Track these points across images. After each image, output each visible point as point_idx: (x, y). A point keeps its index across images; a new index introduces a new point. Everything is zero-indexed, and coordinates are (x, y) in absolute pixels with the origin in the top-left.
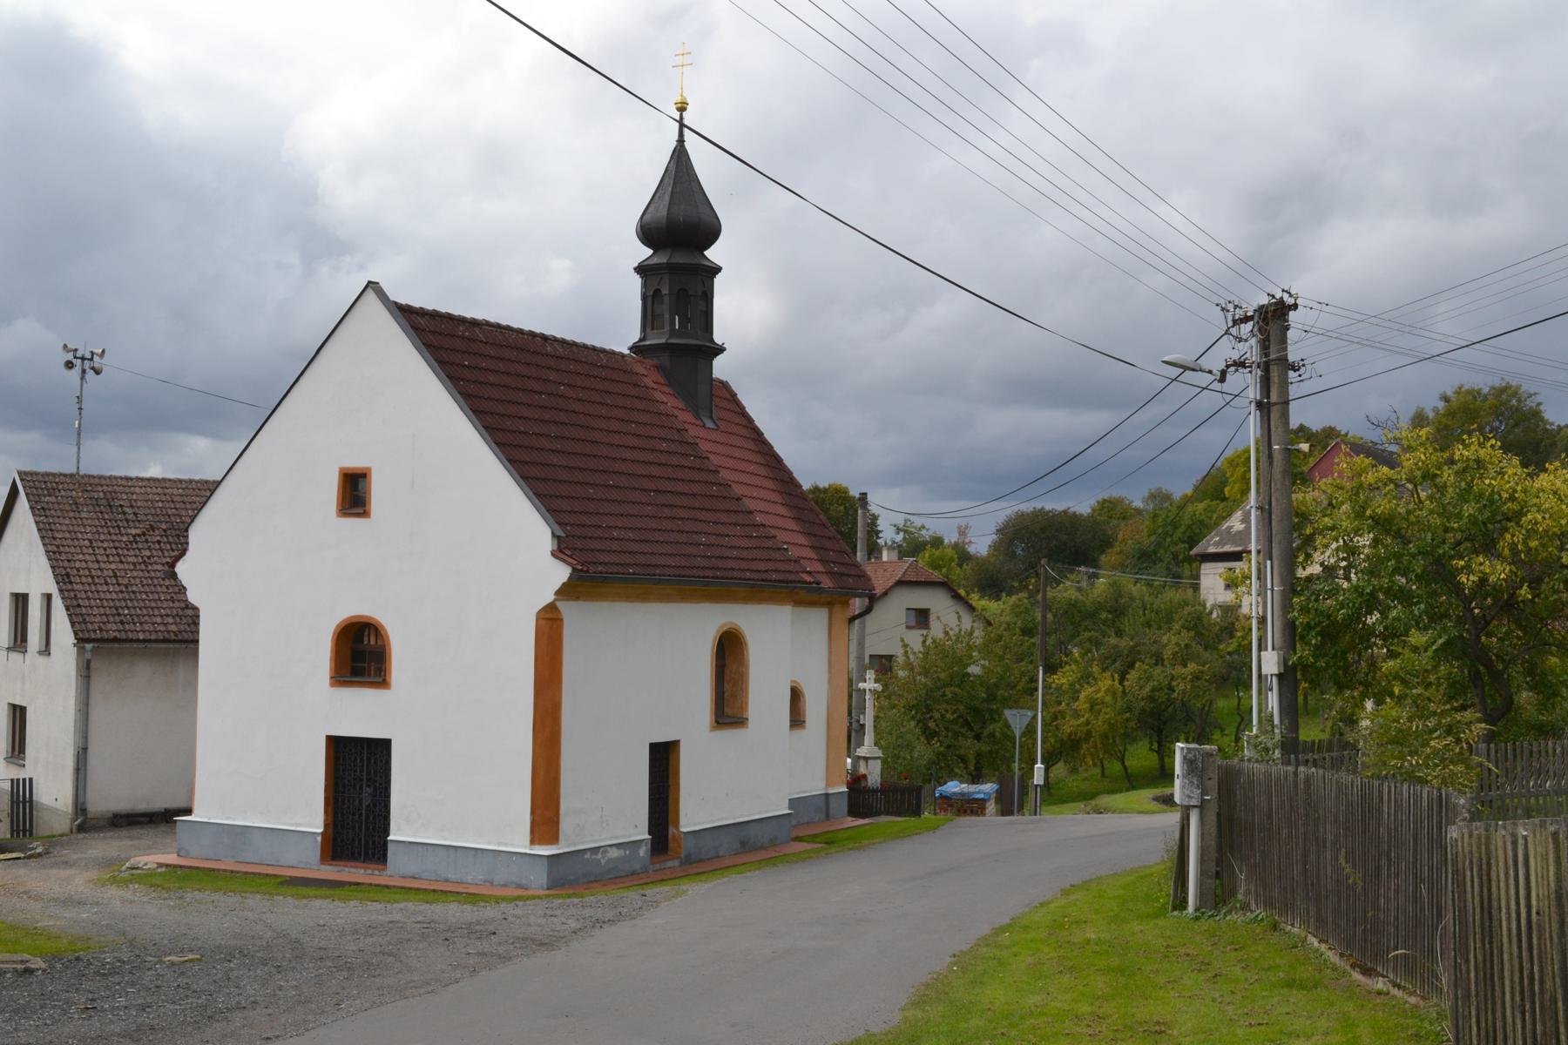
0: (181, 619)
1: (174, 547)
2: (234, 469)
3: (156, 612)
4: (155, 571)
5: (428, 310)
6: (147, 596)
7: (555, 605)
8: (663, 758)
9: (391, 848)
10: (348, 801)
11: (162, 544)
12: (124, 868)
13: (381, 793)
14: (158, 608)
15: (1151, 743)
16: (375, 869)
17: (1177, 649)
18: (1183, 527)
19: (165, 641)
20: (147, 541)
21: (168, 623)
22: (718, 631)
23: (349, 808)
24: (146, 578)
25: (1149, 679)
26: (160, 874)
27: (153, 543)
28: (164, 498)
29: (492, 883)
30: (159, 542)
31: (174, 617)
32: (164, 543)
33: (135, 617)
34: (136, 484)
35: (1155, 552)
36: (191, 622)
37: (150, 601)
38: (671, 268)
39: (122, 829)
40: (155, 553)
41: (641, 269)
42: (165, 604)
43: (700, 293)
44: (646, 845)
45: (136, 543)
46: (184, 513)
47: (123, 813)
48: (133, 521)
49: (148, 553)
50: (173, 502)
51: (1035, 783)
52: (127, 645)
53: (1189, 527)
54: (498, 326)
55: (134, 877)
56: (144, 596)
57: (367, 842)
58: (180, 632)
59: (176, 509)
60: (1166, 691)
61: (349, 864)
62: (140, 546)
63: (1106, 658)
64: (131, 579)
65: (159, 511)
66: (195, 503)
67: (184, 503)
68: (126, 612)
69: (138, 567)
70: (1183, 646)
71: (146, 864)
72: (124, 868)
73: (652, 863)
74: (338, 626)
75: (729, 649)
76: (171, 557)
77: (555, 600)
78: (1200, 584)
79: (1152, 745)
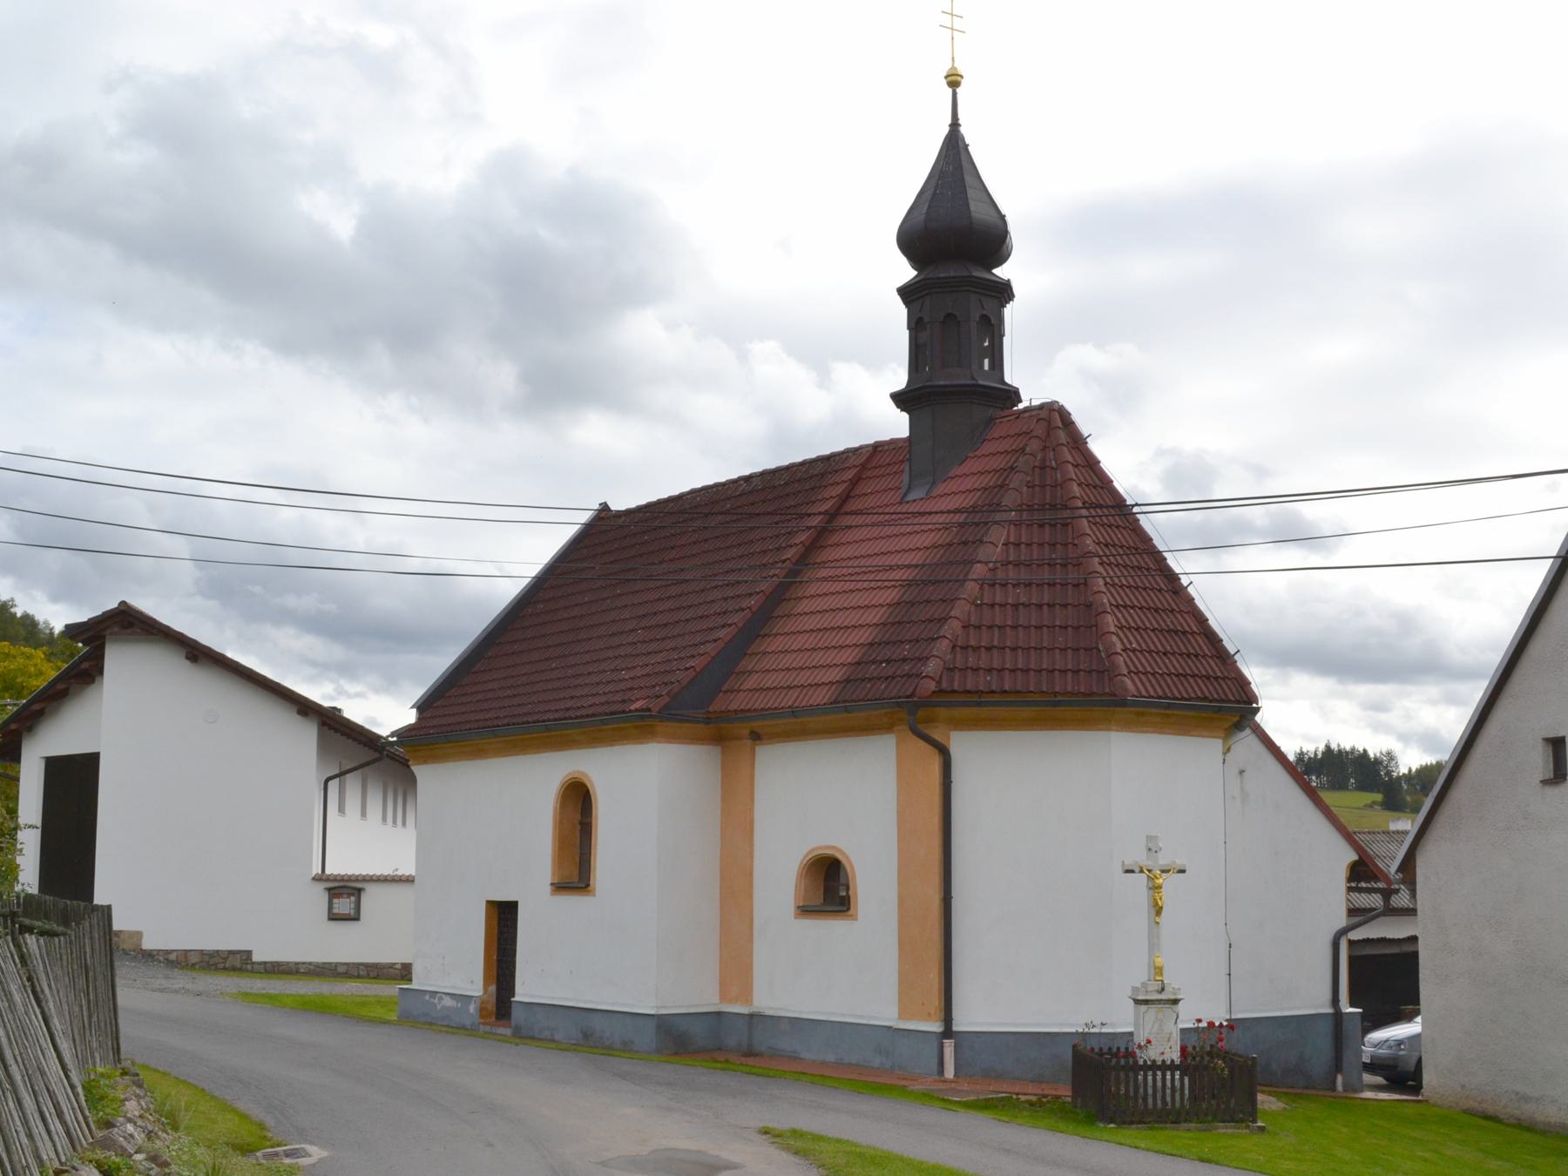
8: (503, 917)
41: (906, 293)
75: (577, 799)
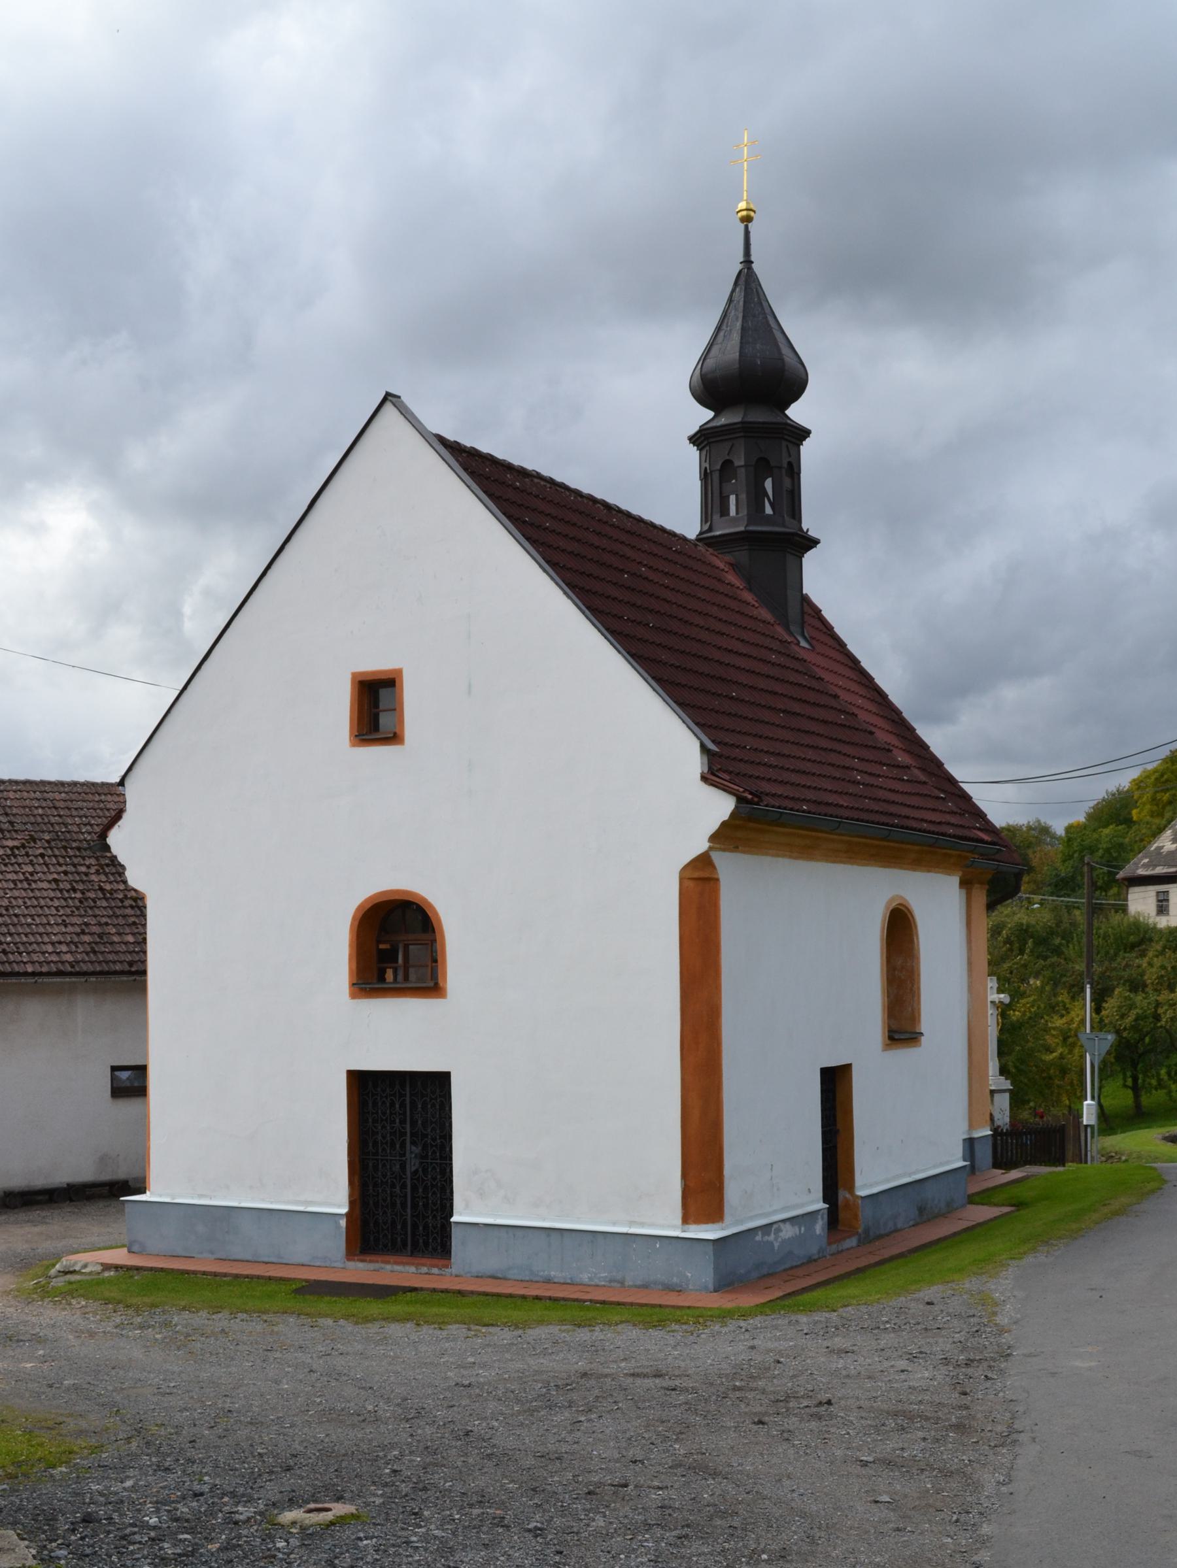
0: (77, 947)
1: (61, 860)
2: (231, 627)
3: (46, 939)
4: (39, 890)
5: (465, 447)
6: (33, 920)
7: (709, 854)
9: (456, 1236)
10: (384, 1165)
11: (46, 858)
12: (53, 1272)
13: (434, 1152)
14: (47, 934)
15: (1125, 1080)
16: (434, 1266)
17: (1163, 973)
18: (1101, 851)
19: (60, 973)
20: (27, 855)
21: (61, 952)
22: (887, 907)
23: (384, 1176)
24: (30, 898)
25: (1132, 1007)
26: (109, 1281)
27: (36, 856)
28: (44, 804)
29: (622, 1283)
30: (42, 855)
31: (67, 944)
32: (49, 856)
33: (20, 945)
34: (9, 788)
35: (1073, 878)
36: (89, 949)
37: (37, 925)
38: (746, 430)
39: (16, 1211)
40: (38, 868)
41: (701, 438)
42: (56, 930)
43: (785, 465)
44: (822, 1219)
45: (15, 857)
46: (69, 821)
47: (17, 1190)
48: (9, 831)
49: (30, 869)
50: (56, 808)
51: (1085, 1123)
52: (14, 980)
53: (1107, 850)
54: (551, 481)
55: (74, 1286)
56: (29, 920)
57: (415, 1226)
58: (78, 962)
59: (60, 816)
60: (1151, 1020)
61: (392, 1258)
62: (20, 860)
63: (1073, 986)
64: (12, 900)
65: (39, 819)
66: (82, 809)
67: (69, 809)
68: (9, 939)
69: (20, 886)
70: (1169, 969)
71: (85, 1266)
72: (53, 1272)
73: (830, 1243)
74: (358, 909)
76: (106, 817)
77: (710, 848)
78: (1127, 905)
79: (1125, 1081)
